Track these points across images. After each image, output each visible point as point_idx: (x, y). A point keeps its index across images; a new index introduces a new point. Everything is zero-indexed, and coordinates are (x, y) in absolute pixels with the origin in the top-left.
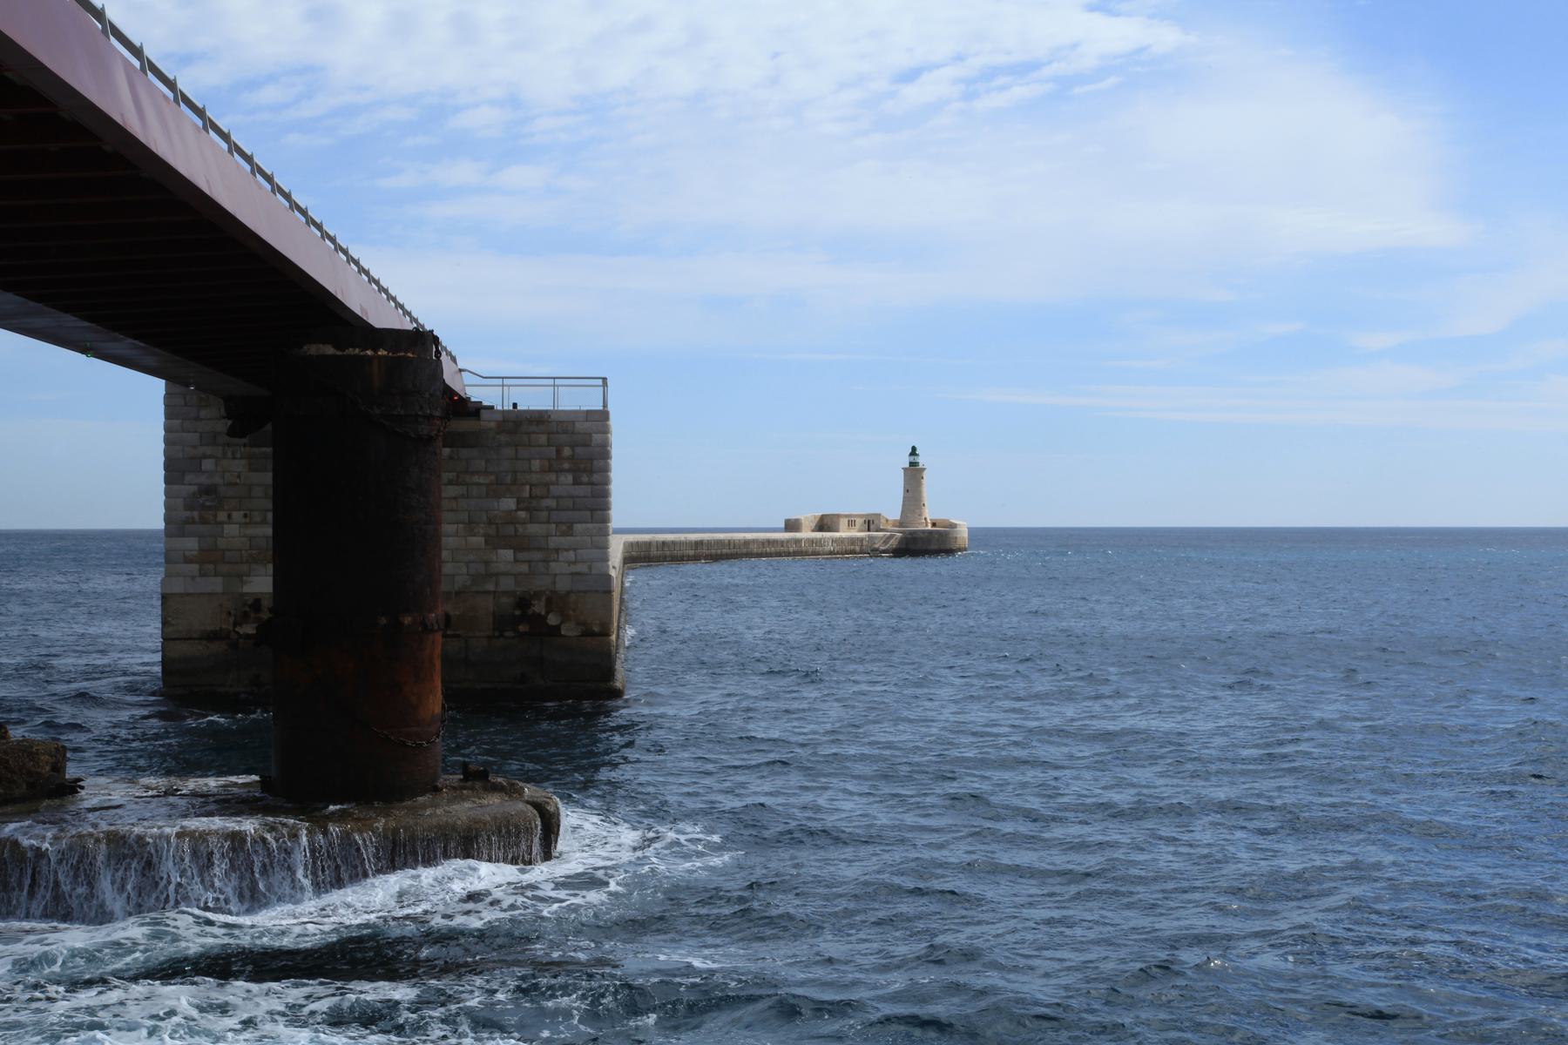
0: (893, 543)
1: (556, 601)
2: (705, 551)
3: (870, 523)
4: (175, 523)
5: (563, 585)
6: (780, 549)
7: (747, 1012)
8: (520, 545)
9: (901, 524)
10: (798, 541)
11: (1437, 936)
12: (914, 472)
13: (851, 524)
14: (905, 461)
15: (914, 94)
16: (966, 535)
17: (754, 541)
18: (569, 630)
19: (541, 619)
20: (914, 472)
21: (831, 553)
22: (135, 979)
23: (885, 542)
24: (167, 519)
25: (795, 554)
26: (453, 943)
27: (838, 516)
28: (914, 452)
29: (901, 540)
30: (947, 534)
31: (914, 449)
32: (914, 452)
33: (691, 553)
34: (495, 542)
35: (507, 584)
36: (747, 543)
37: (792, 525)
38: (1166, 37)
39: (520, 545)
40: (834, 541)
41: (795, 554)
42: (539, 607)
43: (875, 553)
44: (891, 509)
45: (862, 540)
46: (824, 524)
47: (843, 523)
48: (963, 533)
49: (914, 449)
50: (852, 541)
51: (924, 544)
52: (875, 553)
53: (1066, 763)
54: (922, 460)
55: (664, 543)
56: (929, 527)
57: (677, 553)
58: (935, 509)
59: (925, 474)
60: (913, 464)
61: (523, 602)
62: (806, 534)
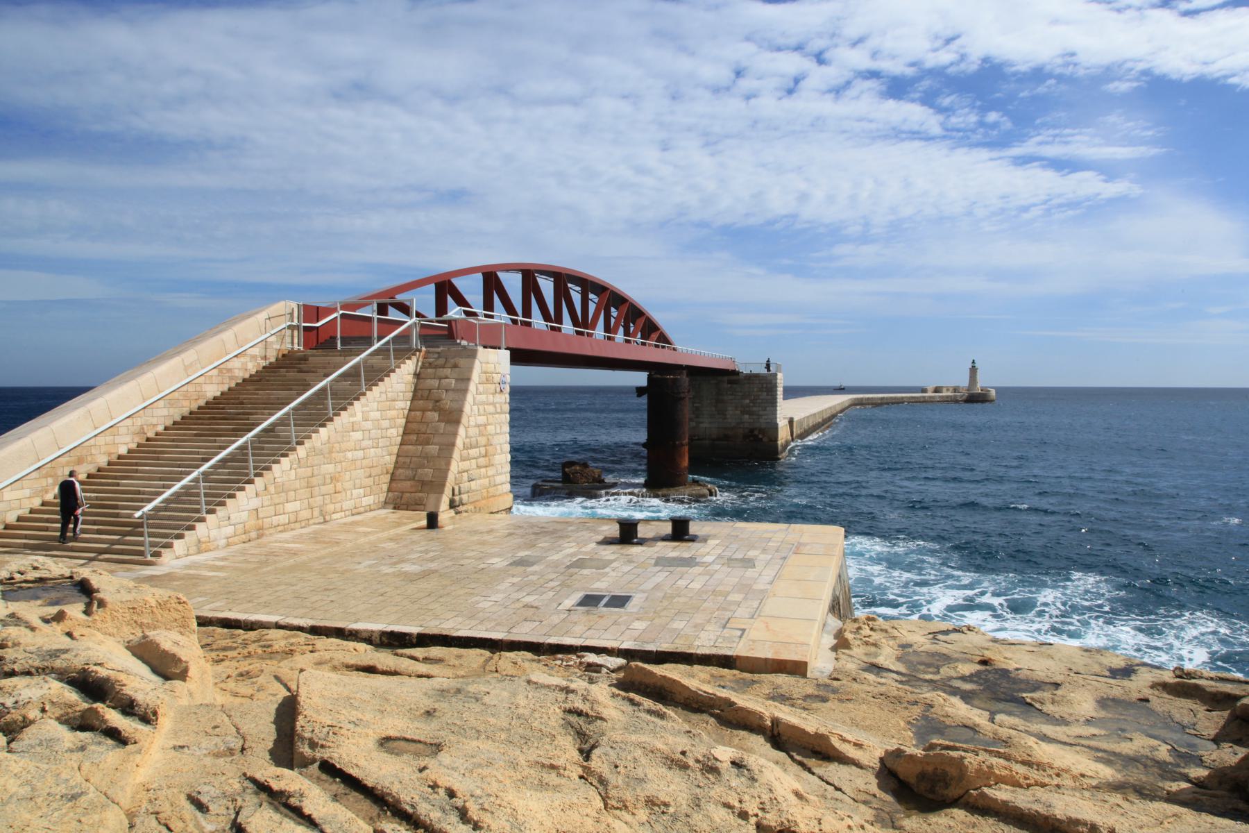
1: (762, 431)
3: (955, 390)
5: (763, 426)
8: (751, 413)
12: (973, 370)
15: (1026, 216)
18: (765, 439)
19: (756, 436)
20: (973, 370)
26: (1168, 677)
34: (743, 413)
35: (746, 425)
38: (1136, 190)
39: (751, 413)
42: (756, 432)
43: (956, 402)
44: (964, 382)
46: (937, 390)
51: (976, 399)
52: (956, 402)
58: (983, 382)
61: (752, 431)
62: (930, 394)
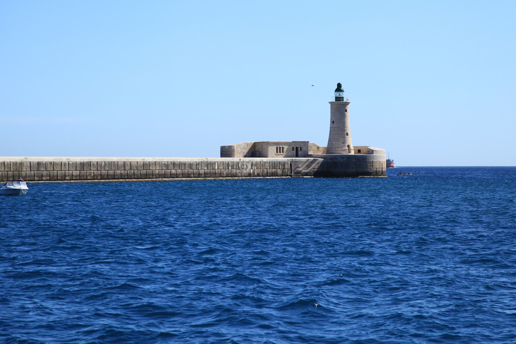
0: (315, 166)
3: (299, 149)
7: (425, 339)
9: (328, 150)
11: (318, 327)
12: (339, 108)
14: (332, 97)
20: (339, 108)
22: (147, 280)
23: (308, 166)
27: (268, 144)
28: (339, 88)
29: (322, 164)
31: (339, 85)
32: (339, 88)
37: (226, 152)
44: (319, 138)
45: (284, 164)
46: (256, 150)
47: (272, 150)
49: (339, 85)
51: (345, 167)
54: (346, 96)
59: (348, 108)
60: (338, 99)
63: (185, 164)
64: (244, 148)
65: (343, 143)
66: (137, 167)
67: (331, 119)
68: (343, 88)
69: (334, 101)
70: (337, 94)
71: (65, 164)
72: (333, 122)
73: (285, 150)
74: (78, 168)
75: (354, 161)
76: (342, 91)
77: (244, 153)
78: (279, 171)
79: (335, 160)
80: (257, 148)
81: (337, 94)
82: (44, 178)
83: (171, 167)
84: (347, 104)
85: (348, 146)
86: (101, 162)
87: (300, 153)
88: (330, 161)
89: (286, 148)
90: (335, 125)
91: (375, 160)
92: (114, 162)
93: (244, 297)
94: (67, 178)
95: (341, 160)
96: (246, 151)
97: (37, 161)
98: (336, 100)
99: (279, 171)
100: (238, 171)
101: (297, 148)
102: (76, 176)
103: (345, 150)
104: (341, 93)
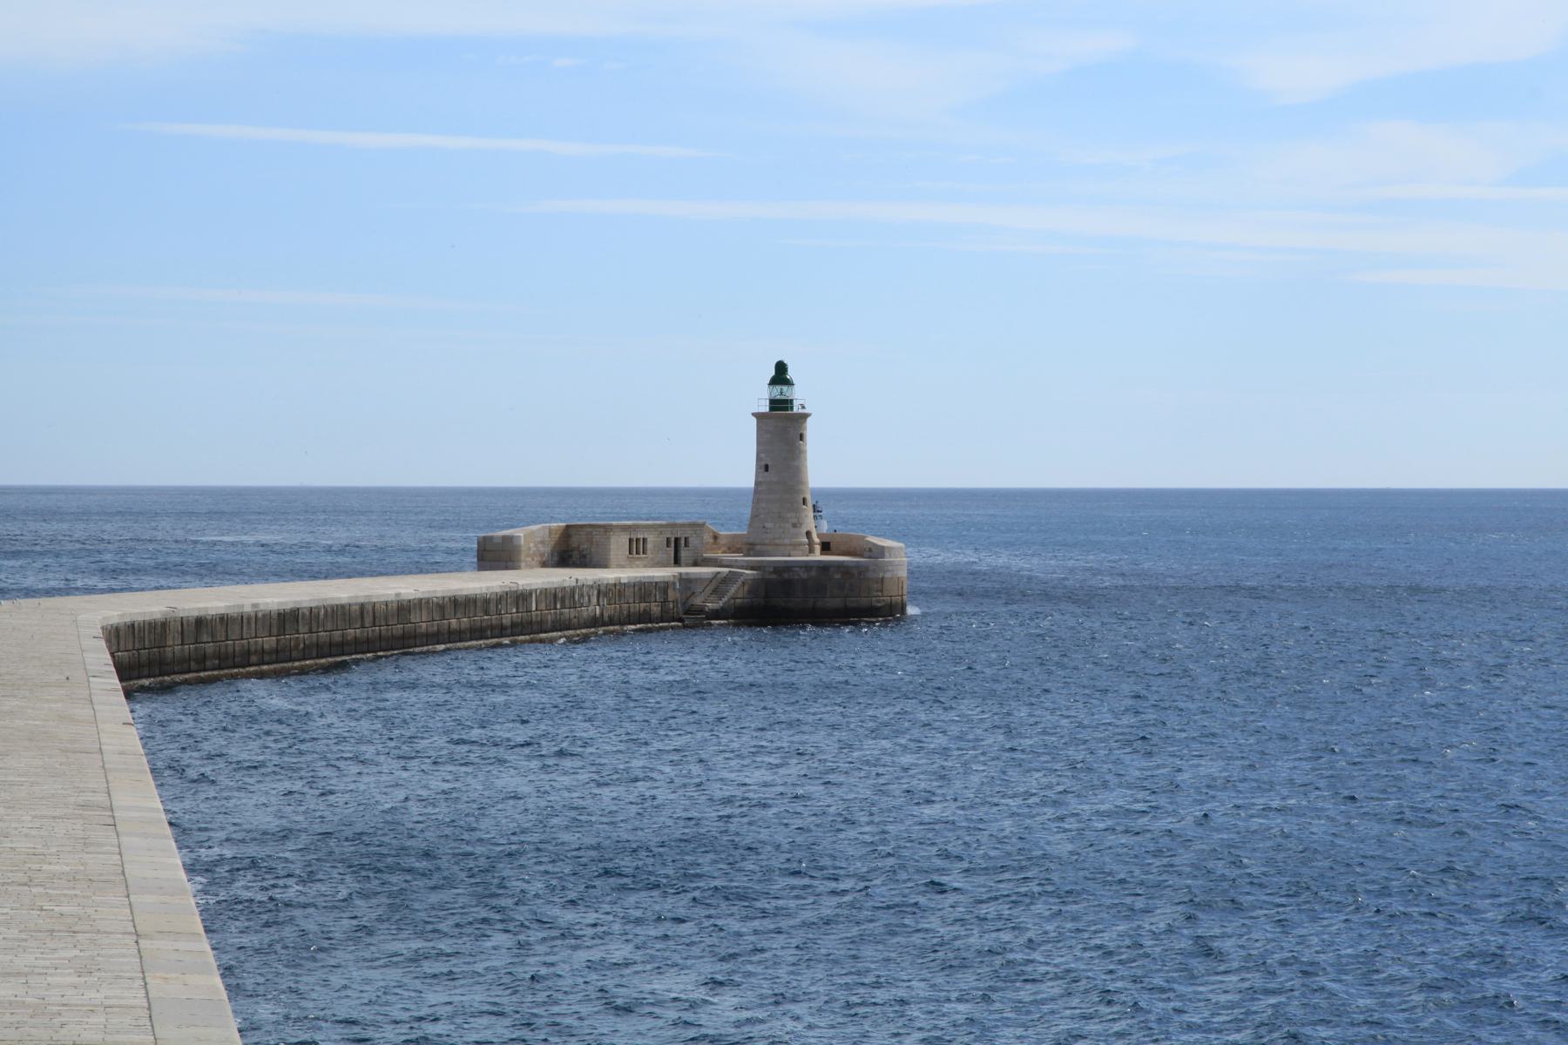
2: (304, 636)
4: (756, 491)
6: (481, 618)
10: (521, 598)
12: (781, 425)
13: (637, 547)
16: (903, 573)
17: (421, 604)
20: (781, 425)
21: (595, 622)
24: (757, 483)
25: (518, 628)
27: (607, 529)
28: (781, 375)
29: (756, 587)
30: (861, 570)
31: (781, 368)
32: (781, 375)
33: (269, 642)
36: (404, 609)
40: (604, 591)
41: (518, 628)
45: (664, 587)
46: (570, 549)
47: (618, 545)
48: (902, 558)
49: (781, 368)
50: (644, 590)
53: (1441, 984)
54: (801, 394)
55: (200, 622)
56: (818, 556)
57: (234, 645)
59: (811, 428)
62: (534, 578)
63: (475, 601)
64: (542, 542)
65: (794, 526)
66: (386, 619)
67: (759, 459)
68: (791, 374)
69: (767, 409)
70: (776, 392)
71: (249, 619)
72: (767, 468)
73: (649, 546)
74: (275, 631)
75: (837, 576)
76: (788, 383)
77: (542, 555)
78: (655, 609)
79: (786, 576)
80: (574, 542)
81: (776, 392)
82: (208, 663)
83: (449, 611)
84: (805, 416)
85: (808, 534)
86: (318, 608)
87: (684, 554)
88: (774, 576)
89: (651, 538)
90: (771, 476)
91: (888, 575)
92: (343, 606)
93: (1270, 809)
94: (254, 659)
95: (804, 576)
96: (547, 549)
97: (196, 614)
98: (772, 409)
99: (655, 609)
100: (573, 613)
101: (677, 540)
102: (270, 652)
103: (801, 544)
104: (785, 388)
